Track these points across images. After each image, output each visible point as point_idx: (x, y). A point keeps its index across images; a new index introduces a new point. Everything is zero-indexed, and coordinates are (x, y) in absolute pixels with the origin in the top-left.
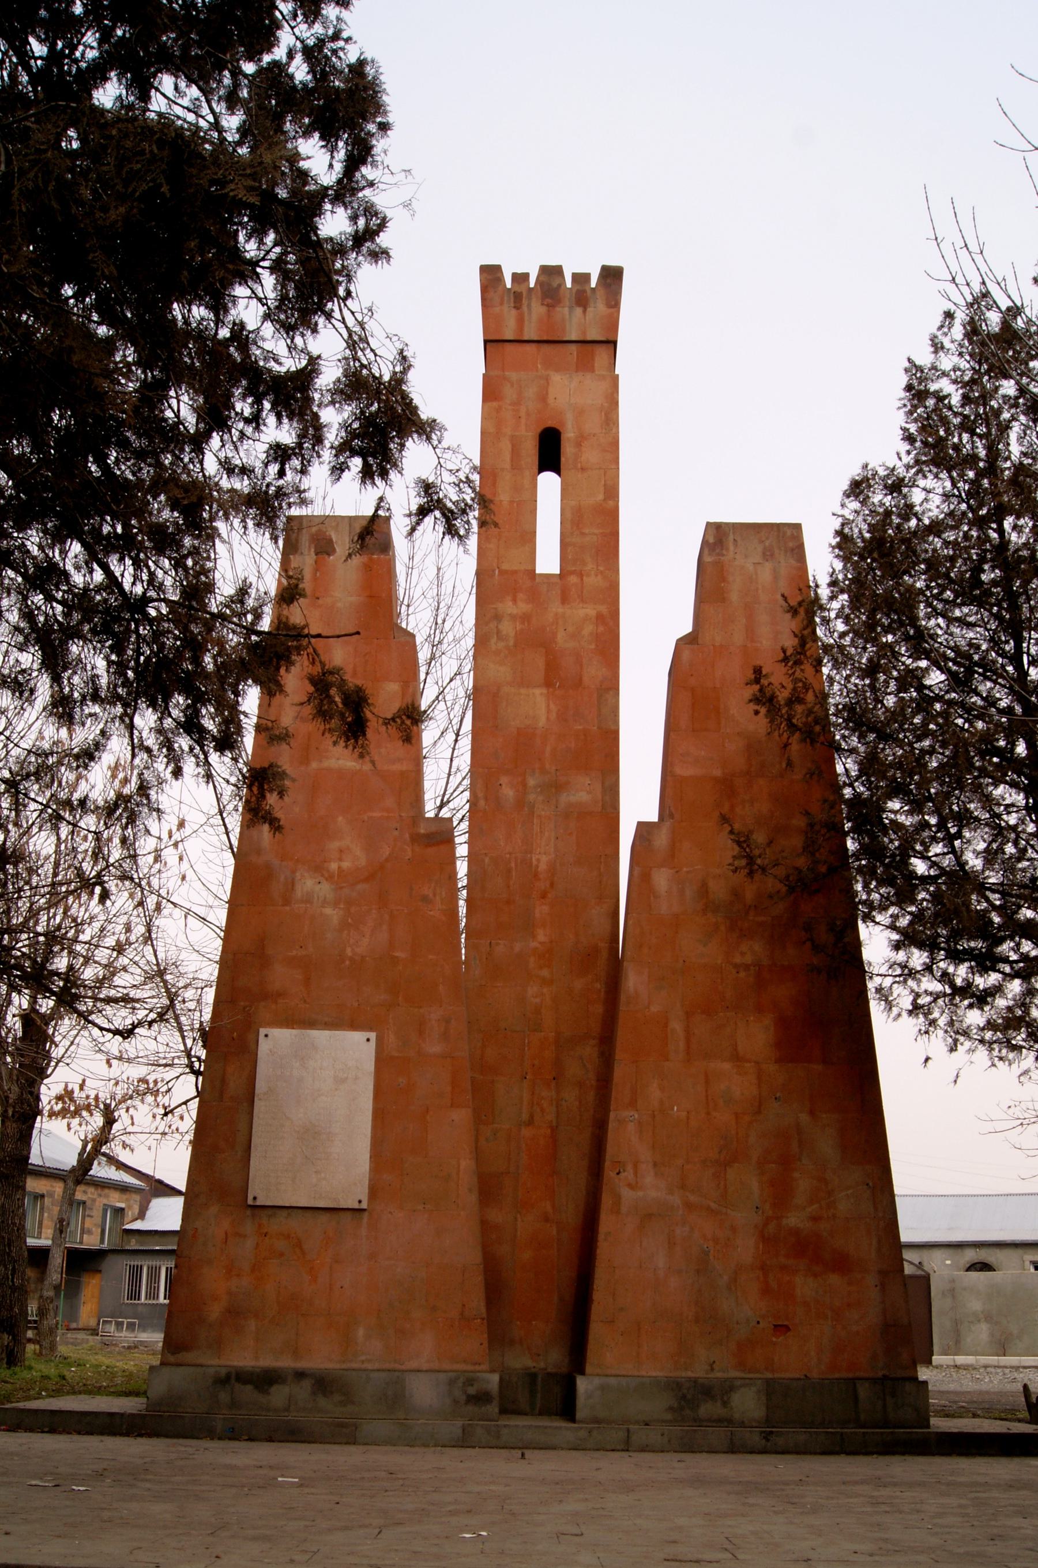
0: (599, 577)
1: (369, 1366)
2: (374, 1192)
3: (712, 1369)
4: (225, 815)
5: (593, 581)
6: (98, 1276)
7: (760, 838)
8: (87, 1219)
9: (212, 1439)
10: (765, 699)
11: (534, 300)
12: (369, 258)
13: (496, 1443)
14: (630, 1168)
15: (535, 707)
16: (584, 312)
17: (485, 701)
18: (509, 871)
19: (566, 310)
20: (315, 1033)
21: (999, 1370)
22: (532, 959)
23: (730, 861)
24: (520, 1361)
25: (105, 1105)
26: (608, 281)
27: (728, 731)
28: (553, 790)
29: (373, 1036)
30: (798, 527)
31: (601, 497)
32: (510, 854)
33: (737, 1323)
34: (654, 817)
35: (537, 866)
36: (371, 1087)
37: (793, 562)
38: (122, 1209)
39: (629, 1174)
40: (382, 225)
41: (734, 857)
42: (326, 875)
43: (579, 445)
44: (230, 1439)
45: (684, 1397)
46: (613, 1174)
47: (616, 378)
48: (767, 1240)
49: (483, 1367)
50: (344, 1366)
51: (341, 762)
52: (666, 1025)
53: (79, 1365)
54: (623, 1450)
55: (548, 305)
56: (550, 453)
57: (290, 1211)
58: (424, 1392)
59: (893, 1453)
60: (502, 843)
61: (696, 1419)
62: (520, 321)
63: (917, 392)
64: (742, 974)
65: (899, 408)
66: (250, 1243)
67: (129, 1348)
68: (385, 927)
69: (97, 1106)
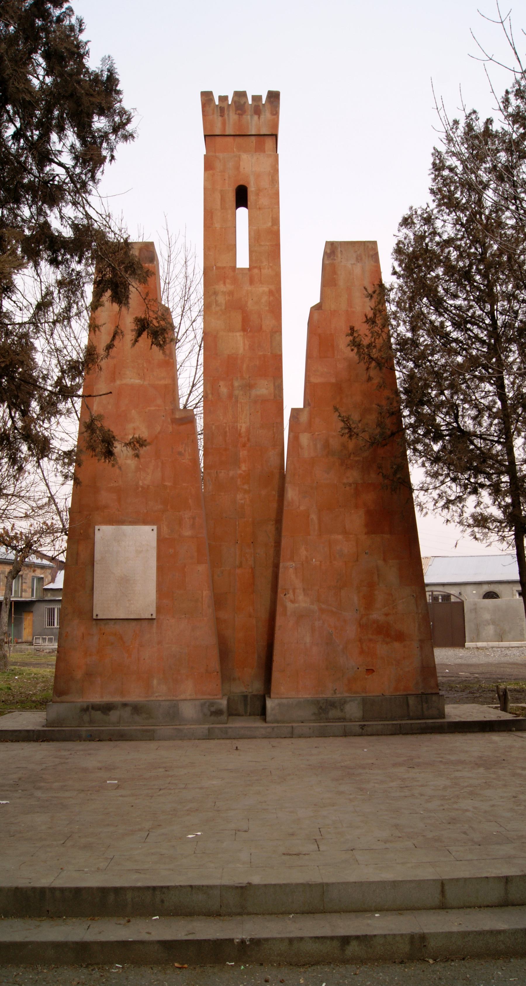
0: (270, 270)
1: (160, 699)
2: (159, 609)
3: (335, 693)
5: (266, 271)
6: (31, 614)
7: (356, 417)
8: (24, 585)
9: (80, 741)
10: (356, 344)
11: (231, 112)
12: (122, 139)
13: (226, 736)
15: (237, 343)
16: (259, 118)
17: (210, 342)
18: (226, 432)
19: (249, 117)
20: (124, 527)
21: (499, 649)
22: (239, 480)
23: (340, 430)
24: (238, 689)
25: (26, 537)
27: (339, 357)
29: (155, 527)
30: (375, 243)
33: (348, 669)
34: (301, 406)
35: (240, 430)
36: (155, 554)
37: (372, 263)
38: (43, 578)
39: (290, 595)
40: (129, 120)
41: (342, 428)
43: (257, 195)
44: (90, 741)
45: (321, 708)
46: (282, 595)
48: (362, 626)
49: (218, 697)
50: (147, 699)
51: (132, 380)
52: (308, 517)
53: (20, 674)
54: (290, 737)
55: (239, 114)
56: (242, 197)
58: (189, 710)
59: (426, 733)
60: (221, 418)
61: (327, 718)
62: (224, 124)
63: (438, 167)
64: (348, 488)
65: (429, 174)
66: (96, 639)
67: (49, 652)
68: (159, 469)
69: (22, 538)
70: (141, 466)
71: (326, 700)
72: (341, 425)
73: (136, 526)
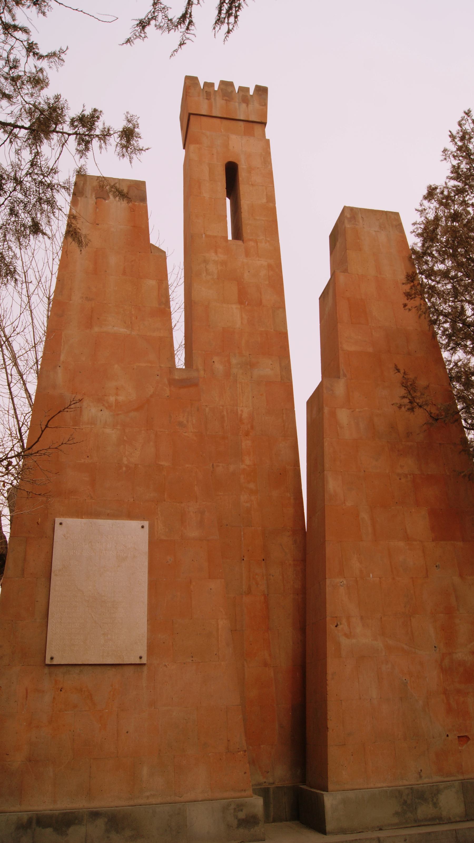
1: (153, 801)
2: (152, 648)
3: (421, 777)
4: (12, 385)
14: (344, 621)
15: (233, 316)
16: (247, 106)
19: (237, 104)
20: (100, 522)
26: (260, 93)
28: (249, 367)
29: (146, 524)
31: (264, 200)
32: (223, 406)
35: (241, 415)
36: (147, 564)
39: (344, 626)
42: (107, 405)
45: (405, 802)
46: (333, 627)
47: (268, 141)
50: (132, 803)
51: (115, 328)
55: (226, 100)
57: (82, 668)
62: (210, 106)
64: (403, 480)
70: (125, 438)
71: (412, 789)
72: (403, 392)
73: (118, 521)
